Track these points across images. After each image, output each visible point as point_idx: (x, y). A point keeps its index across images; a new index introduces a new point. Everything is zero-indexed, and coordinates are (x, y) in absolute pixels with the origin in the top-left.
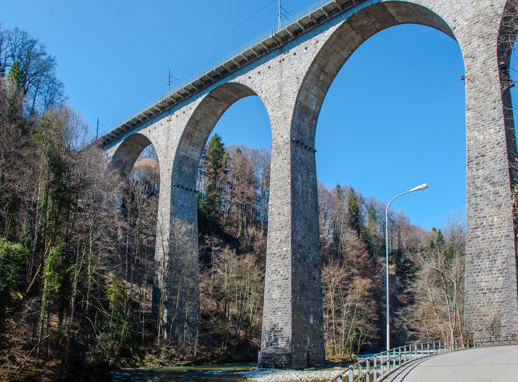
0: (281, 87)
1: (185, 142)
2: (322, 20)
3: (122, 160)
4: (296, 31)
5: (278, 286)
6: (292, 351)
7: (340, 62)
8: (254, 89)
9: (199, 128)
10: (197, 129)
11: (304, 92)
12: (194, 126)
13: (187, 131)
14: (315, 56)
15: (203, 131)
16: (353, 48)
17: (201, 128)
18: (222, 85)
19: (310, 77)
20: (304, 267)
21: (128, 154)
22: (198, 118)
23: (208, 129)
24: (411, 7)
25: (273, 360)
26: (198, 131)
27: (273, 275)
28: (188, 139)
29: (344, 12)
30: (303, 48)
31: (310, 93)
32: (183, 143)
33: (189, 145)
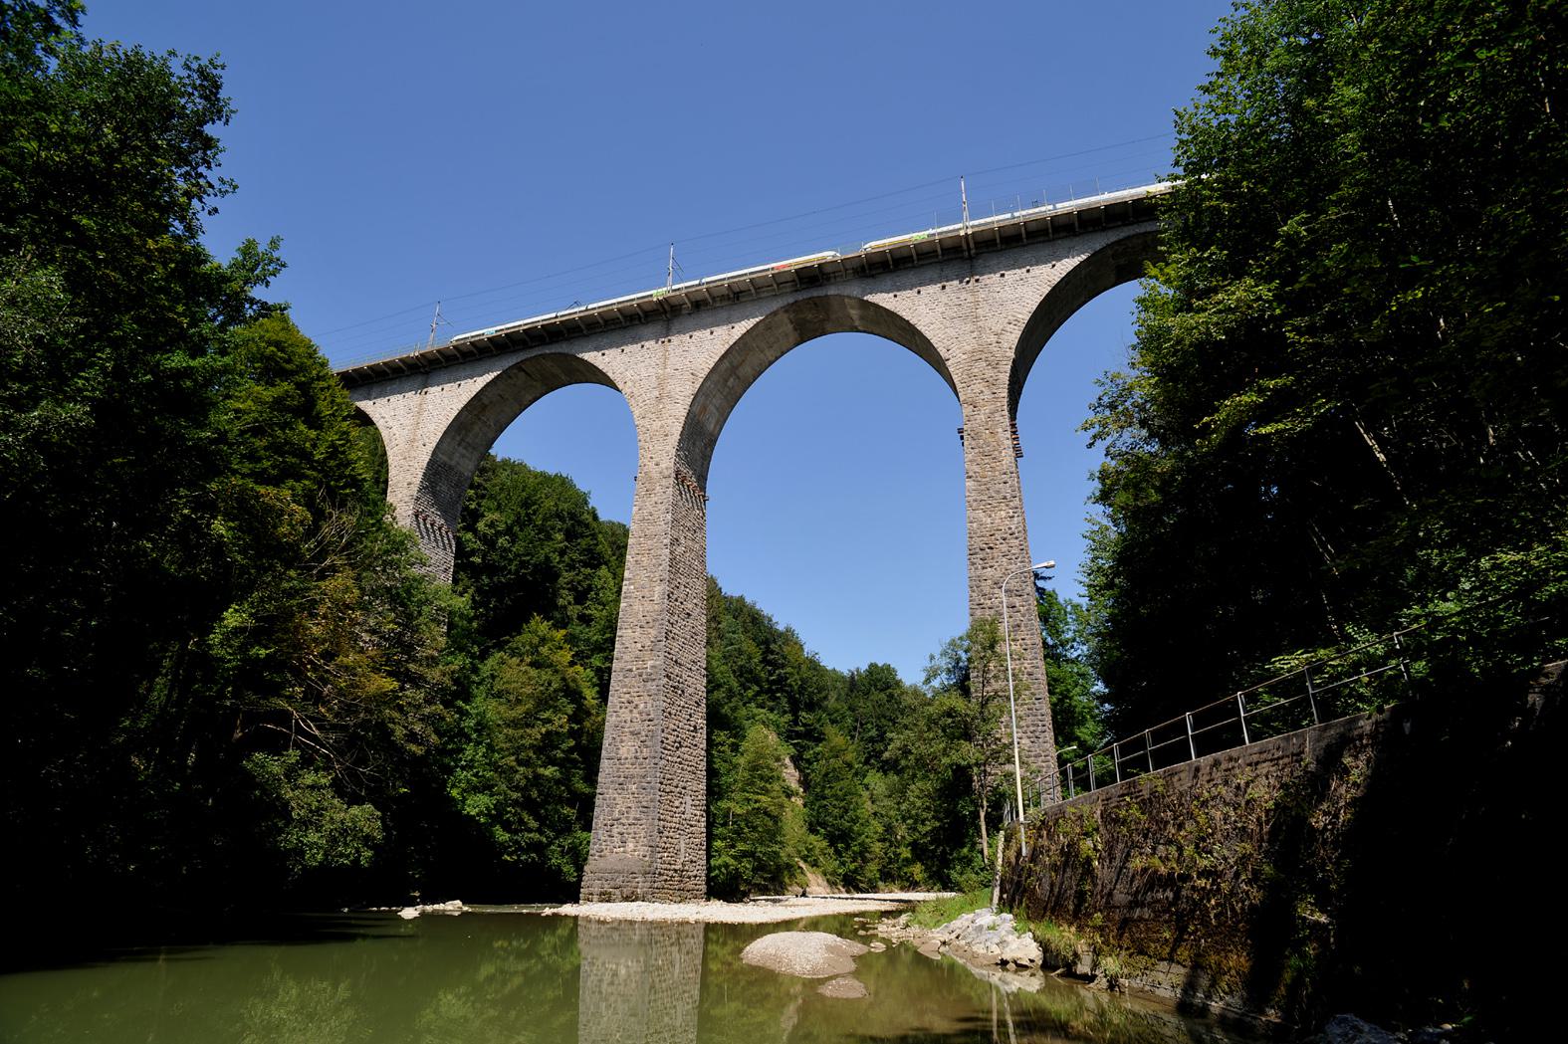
0: (661, 383)
1: (453, 439)
2: (744, 296)
4: (697, 302)
5: (632, 733)
7: (761, 364)
8: (610, 374)
10: (479, 419)
11: (701, 399)
14: (727, 347)
16: (784, 349)
18: (546, 354)
19: (715, 377)
22: (486, 402)
24: (884, 314)
27: (623, 710)
29: (1029, 244)
30: (600, 353)
31: (711, 402)
33: (459, 445)
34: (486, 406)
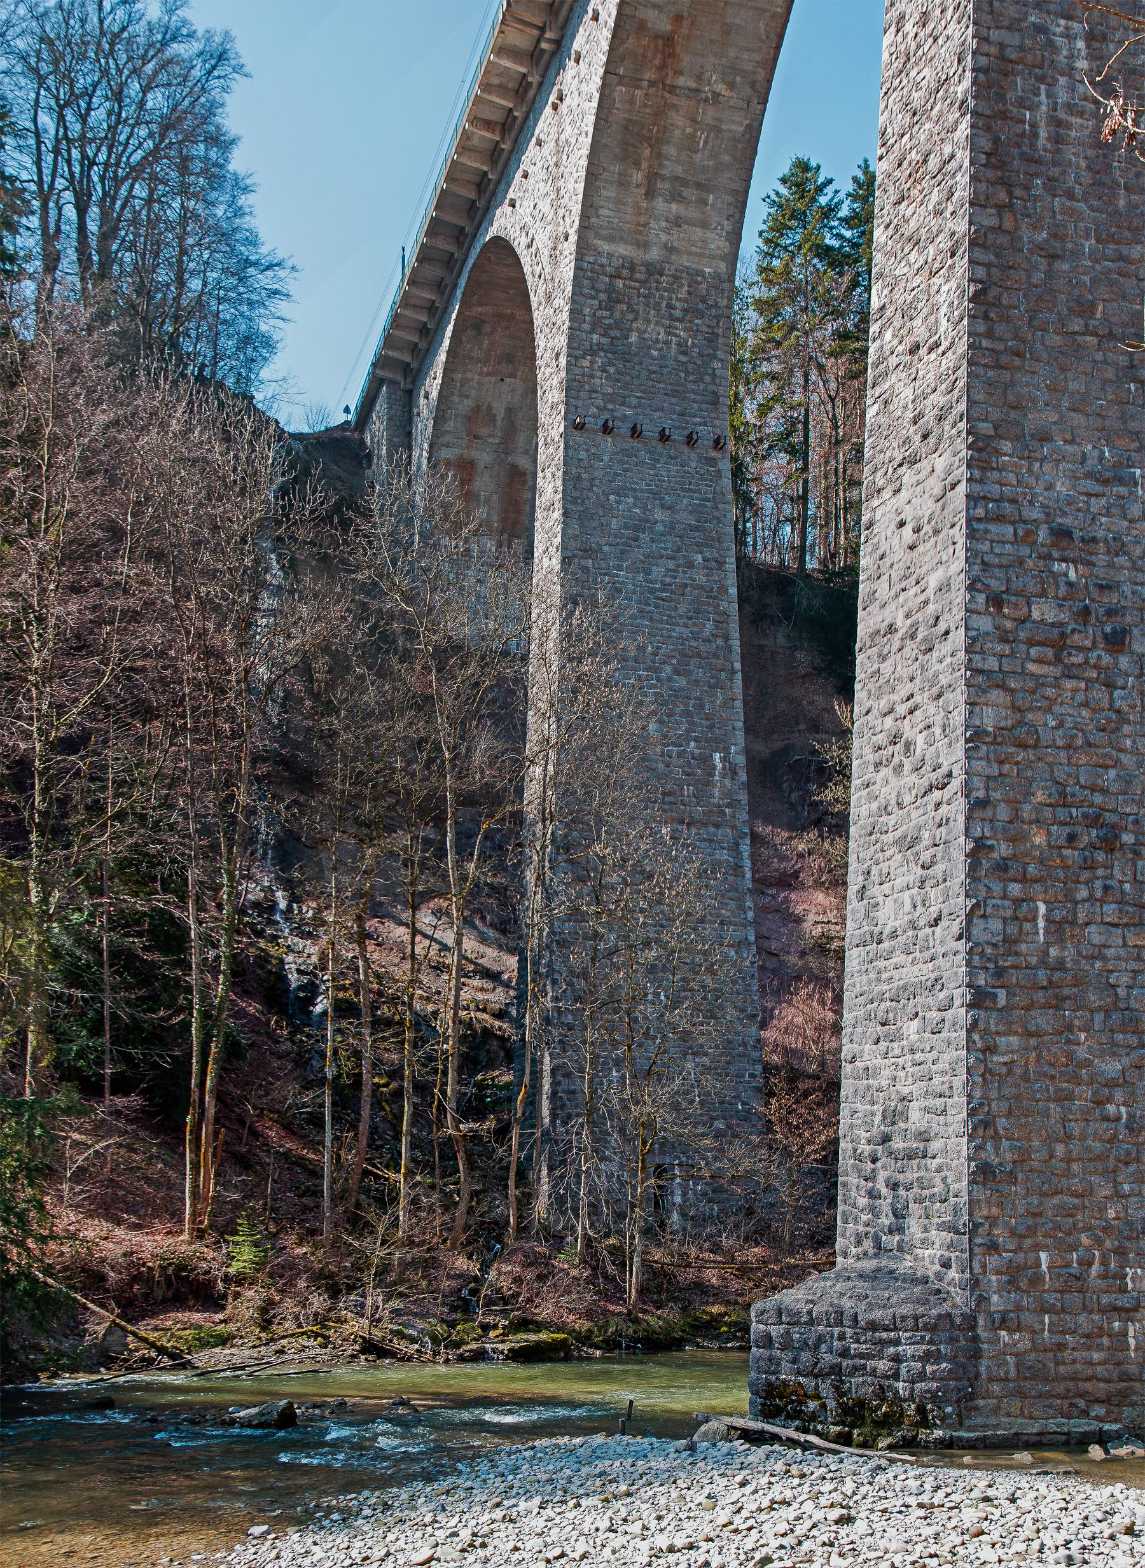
1: (623, 183)
3: (490, 408)
6: (982, 1300)
9: (681, 81)
10: (672, 89)
12: (649, 75)
13: (619, 115)
15: (716, 95)
17: (699, 78)
20: (1110, 686)
21: (505, 368)
23: (742, 73)
25: (828, 1359)
26: (682, 103)
28: (637, 164)
32: (609, 192)
33: (650, 194)
34: (668, 41)
